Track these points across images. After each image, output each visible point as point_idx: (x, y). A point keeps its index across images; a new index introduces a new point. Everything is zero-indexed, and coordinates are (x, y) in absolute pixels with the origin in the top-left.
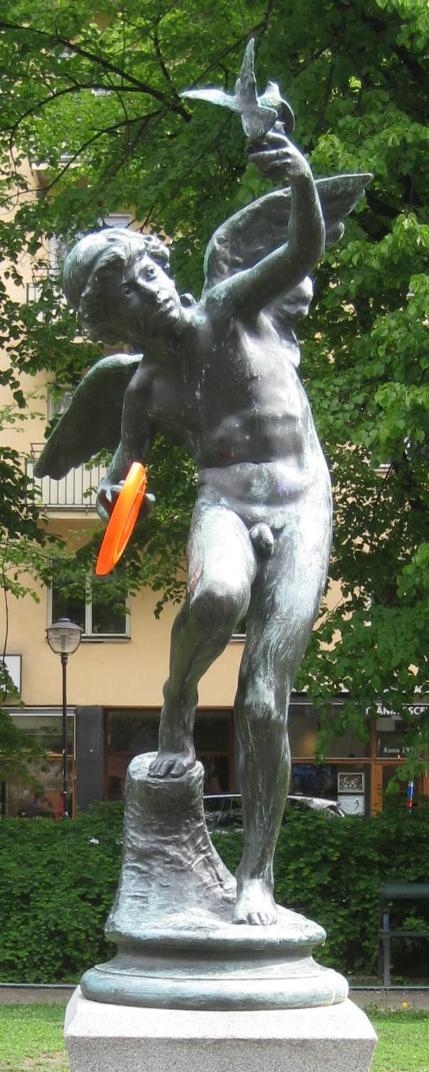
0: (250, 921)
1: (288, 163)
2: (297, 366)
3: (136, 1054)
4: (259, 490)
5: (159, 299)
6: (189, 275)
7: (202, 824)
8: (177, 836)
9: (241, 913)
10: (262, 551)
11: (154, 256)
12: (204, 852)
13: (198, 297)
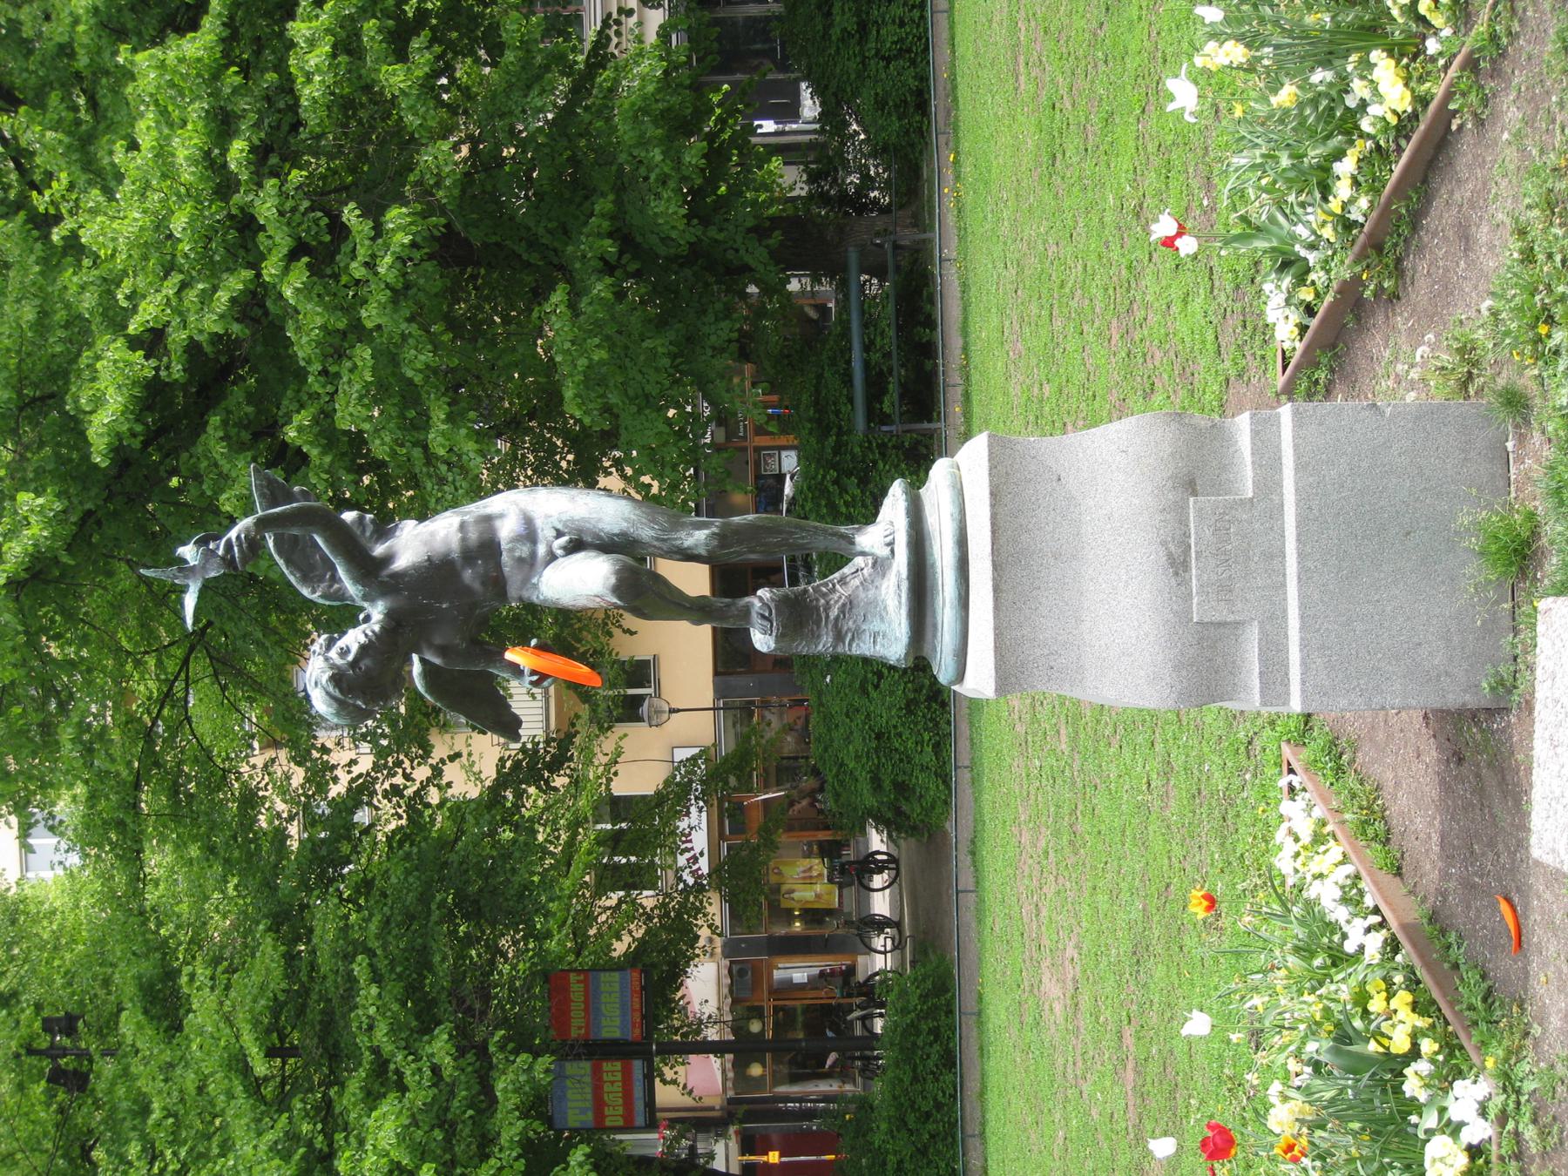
0: (891, 544)
4: (524, 551)
6: (342, 617)
13: (362, 609)
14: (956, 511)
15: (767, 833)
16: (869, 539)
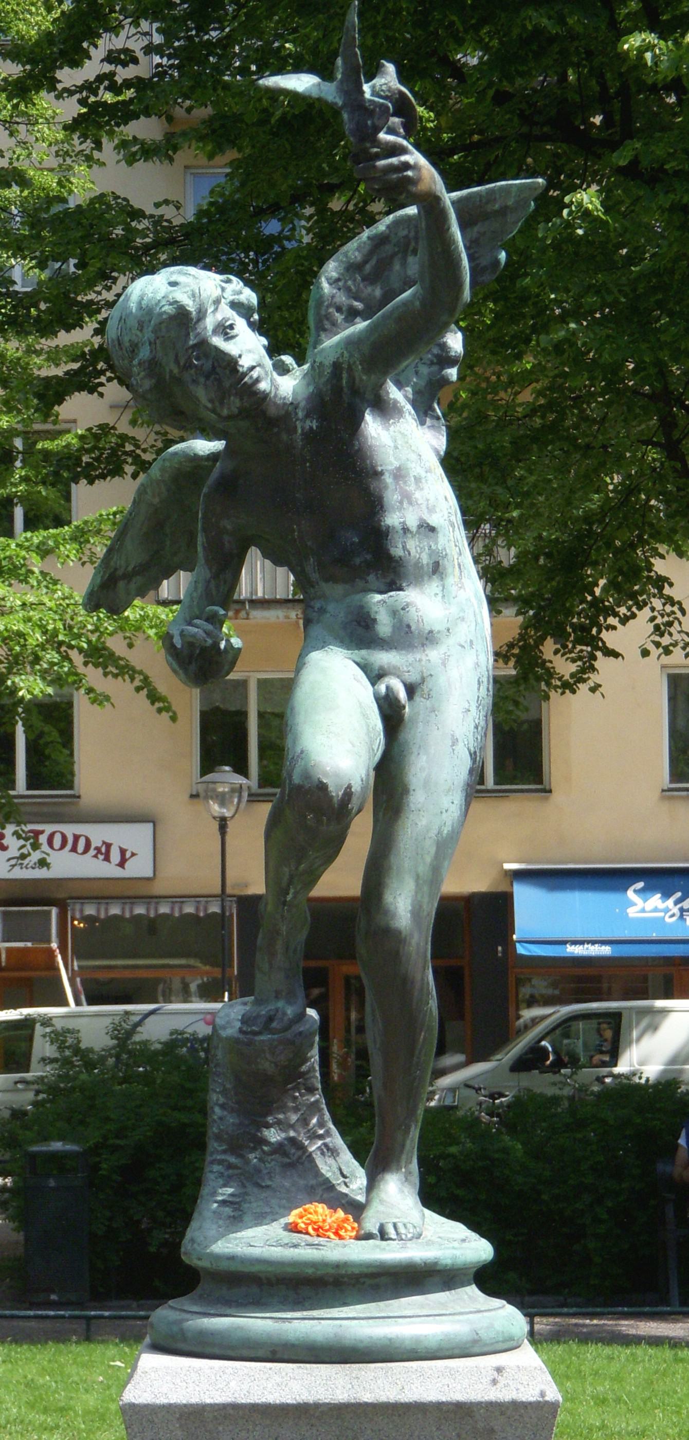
0: (383, 1235)
1: (408, 177)
3: (220, 1428)
4: (384, 626)
5: (243, 367)
6: (285, 330)
7: (318, 1096)
8: (281, 1116)
9: (371, 1224)
10: (392, 716)
11: (234, 305)
12: (321, 1137)
13: (300, 361)
14: (432, 1344)
16: (398, 1197)
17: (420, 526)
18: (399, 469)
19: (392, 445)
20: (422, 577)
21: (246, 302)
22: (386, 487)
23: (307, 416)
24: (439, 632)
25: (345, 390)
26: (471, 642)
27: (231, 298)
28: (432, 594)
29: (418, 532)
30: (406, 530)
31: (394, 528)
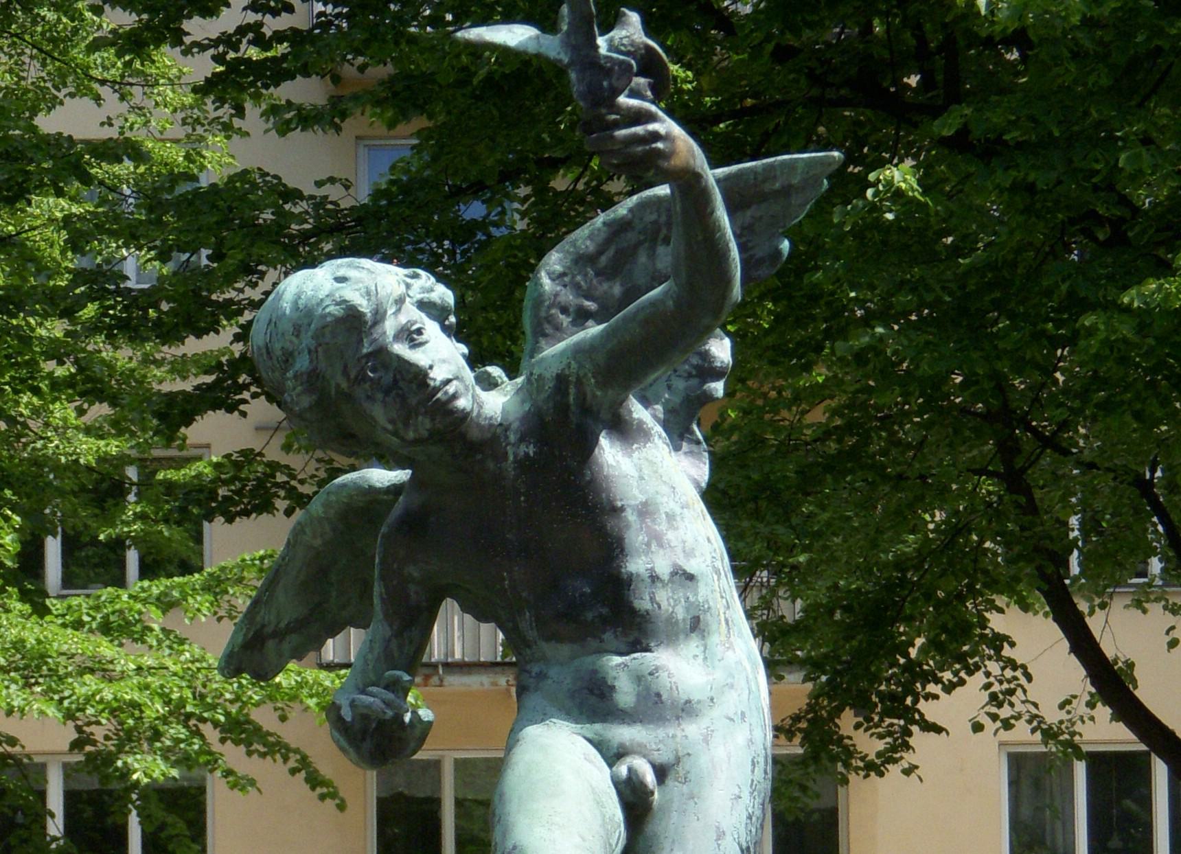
1: (658, 150)
2: (704, 485)
4: (625, 694)
6: (491, 332)
11: (423, 305)
13: (512, 373)
15: (848, 324)
17: (674, 574)
18: (645, 504)
19: (636, 475)
20: (677, 635)
21: (439, 301)
22: (628, 526)
23: (522, 439)
24: (699, 702)
25: (573, 408)
26: (743, 714)
27: (419, 296)
28: (690, 656)
29: (671, 581)
30: (654, 578)
31: (638, 575)
